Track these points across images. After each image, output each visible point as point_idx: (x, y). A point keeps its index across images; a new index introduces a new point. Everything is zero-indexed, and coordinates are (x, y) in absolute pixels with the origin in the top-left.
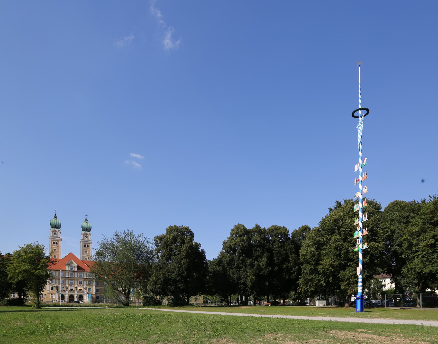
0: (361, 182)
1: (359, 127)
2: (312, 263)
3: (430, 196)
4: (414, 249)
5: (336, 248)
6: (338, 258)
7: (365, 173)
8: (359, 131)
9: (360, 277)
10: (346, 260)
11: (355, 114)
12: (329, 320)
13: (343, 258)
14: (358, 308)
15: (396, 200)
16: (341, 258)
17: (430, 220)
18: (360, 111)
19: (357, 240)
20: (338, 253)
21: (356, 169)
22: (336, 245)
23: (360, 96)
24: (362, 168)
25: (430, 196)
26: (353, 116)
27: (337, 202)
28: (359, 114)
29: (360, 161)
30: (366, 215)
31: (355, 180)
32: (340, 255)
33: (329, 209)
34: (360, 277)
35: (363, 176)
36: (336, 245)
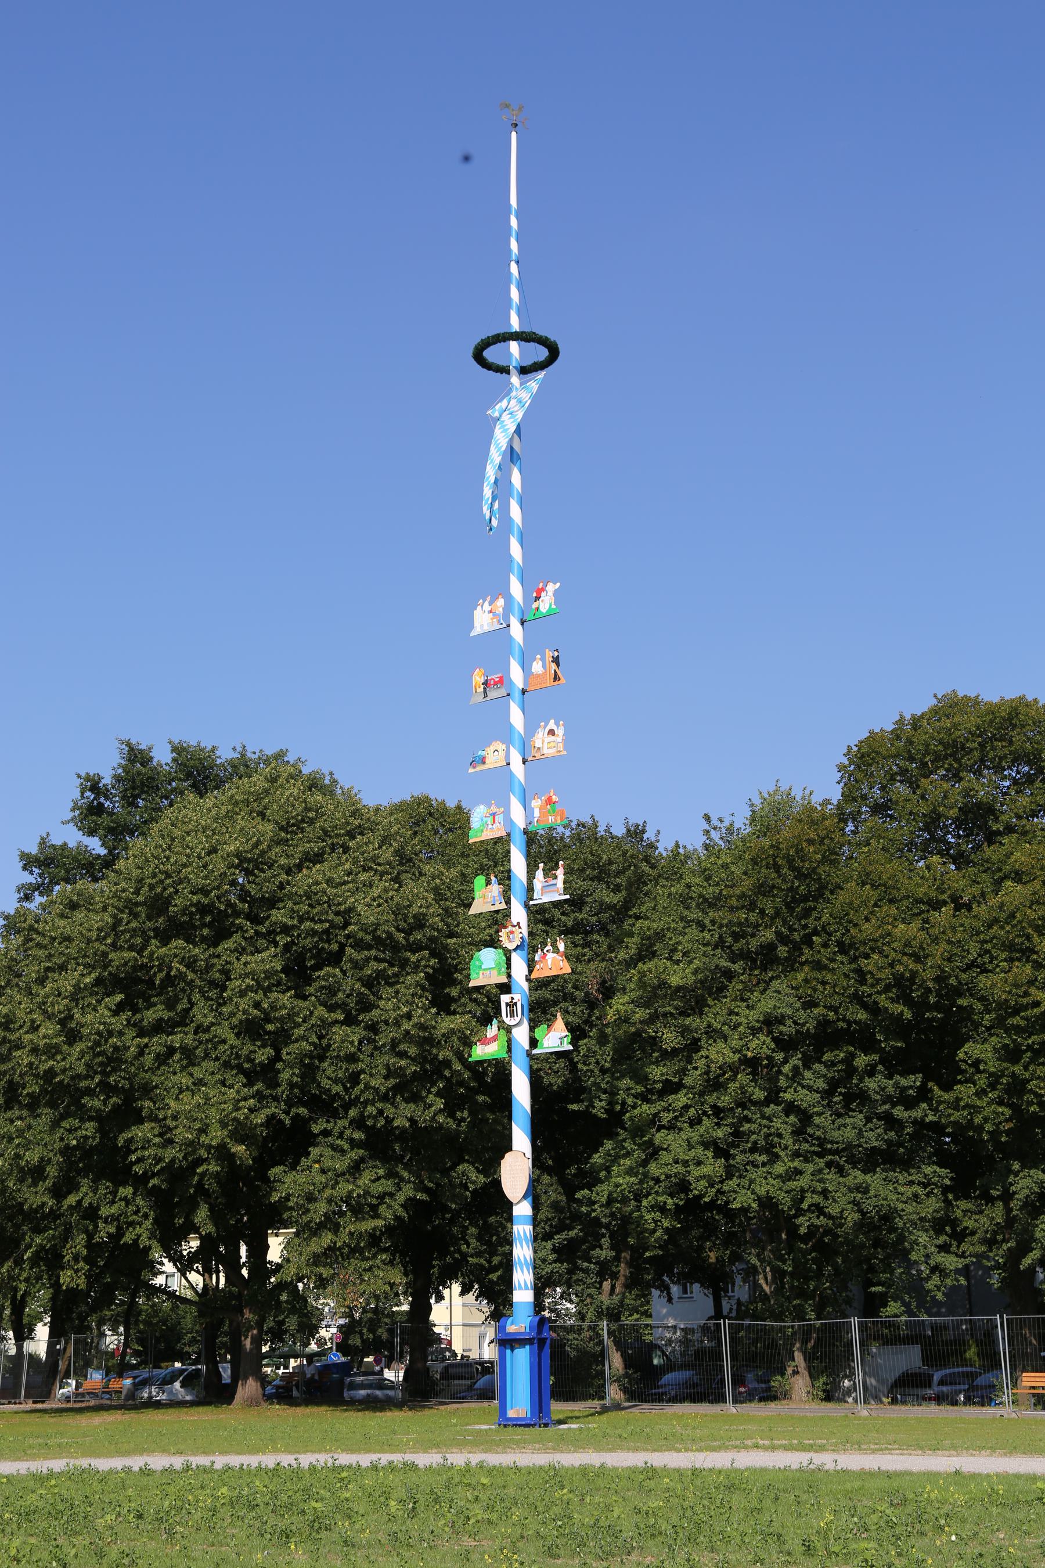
0: (517, 694)
1: (505, 417)
2: (93, 1103)
3: (707, 818)
4: (657, 1072)
5: (251, 1029)
6: (259, 1086)
7: (549, 654)
8: (498, 432)
9: (523, 1210)
10: (301, 1103)
11: (489, 354)
12: (641, 1465)
13: (292, 1086)
14: (519, 1400)
15: (419, 791)
16: (274, 1084)
17: (736, 937)
18: (514, 346)
19: (505, 998)
20: (263, 1055)
21: (483, 620)
22: (257, 1005)
23: (514, 268)
24: (522, 622)
25: (707, 818)
26: (479, 357)
27: (131, 749)
28: (510, 355)
29: (516, 589)
30: (560, 873)
31: (478, 678)
32: (267, 1073)
33: (88, 778)
34: (523, 1210)
35: (537, 667)
36: (257, 1005)
